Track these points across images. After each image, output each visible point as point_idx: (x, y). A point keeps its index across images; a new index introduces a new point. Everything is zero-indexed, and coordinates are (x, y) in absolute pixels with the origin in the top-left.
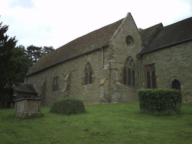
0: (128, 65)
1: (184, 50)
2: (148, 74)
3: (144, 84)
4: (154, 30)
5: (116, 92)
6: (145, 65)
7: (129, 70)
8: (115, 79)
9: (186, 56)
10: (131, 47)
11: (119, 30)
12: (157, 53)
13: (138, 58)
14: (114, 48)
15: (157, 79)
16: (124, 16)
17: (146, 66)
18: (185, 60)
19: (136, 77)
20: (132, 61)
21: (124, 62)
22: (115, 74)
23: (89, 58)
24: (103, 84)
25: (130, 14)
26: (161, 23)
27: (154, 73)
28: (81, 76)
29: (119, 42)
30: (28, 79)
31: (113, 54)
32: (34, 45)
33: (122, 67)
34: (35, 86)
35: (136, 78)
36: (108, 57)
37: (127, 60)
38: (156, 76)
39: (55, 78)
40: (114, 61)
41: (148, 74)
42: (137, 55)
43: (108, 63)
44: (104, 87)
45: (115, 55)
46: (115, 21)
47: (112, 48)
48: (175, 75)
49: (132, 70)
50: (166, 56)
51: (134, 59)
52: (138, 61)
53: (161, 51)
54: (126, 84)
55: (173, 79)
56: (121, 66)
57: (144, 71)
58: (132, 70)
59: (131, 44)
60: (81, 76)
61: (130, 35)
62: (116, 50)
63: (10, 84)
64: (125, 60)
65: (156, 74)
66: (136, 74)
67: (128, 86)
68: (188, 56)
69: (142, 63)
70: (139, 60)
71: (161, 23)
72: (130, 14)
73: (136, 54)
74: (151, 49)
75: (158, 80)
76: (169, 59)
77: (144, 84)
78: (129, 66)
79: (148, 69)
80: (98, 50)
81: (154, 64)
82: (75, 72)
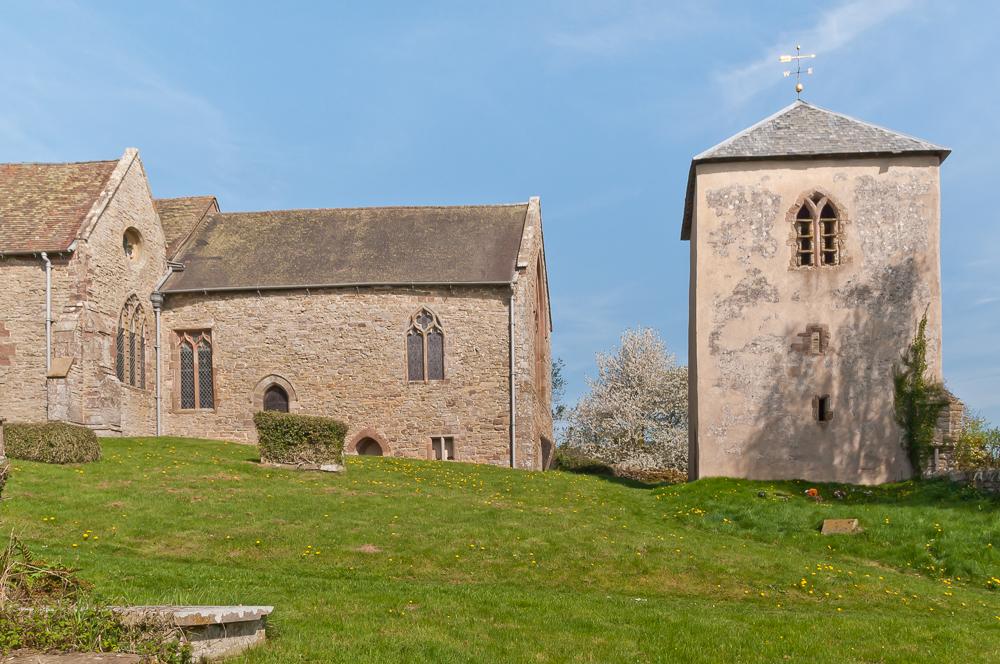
1: (304, 309)
5: (109, 402)
6: (176, 328)
7: (132, 336)
8: (101, 364)
9: (309, 326)
12: (222, 302)
13: (157, 305)
14: (92, 264)
15: (218, 376)
17: (180, 333)
18: (305, 336)
19: (147, 360)
22: (100, 347)
24: (64, 377)
27: (207, 357)
29: (104, 244)
31: (89, 282)
35: (149, 365)
36: (74, 291)
38: (214, 366)
40: (93, 305)
41: (186, 357)
43: (75, 311)
44: (67, 384)
45: (95, 287)
46: (697, 290)
47: (86, 264)
48: (275, 372)
50: (250, 315)
52: (155, 312)
55: (268, 382)
58: (137, 339)
61: (136, 226)
62: (97, 271)
67: (129, 388)
68: (314, 329)
70: (158, 310)
74: (203, 286)
75: (220, 379)
76: (259, 324)
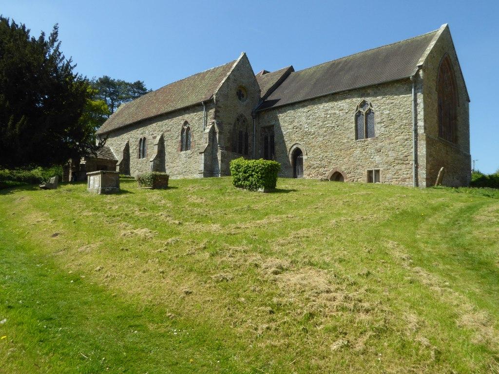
2: (266, 138)
7: (241, 132)
17: (264, 128)
23: (187, 117)
37: (238, 120)
49: (244, 133)
51: (247, 117)
54: (236, 152)
55: (295, 147)
66: (250, 138)
81: (273, 126)
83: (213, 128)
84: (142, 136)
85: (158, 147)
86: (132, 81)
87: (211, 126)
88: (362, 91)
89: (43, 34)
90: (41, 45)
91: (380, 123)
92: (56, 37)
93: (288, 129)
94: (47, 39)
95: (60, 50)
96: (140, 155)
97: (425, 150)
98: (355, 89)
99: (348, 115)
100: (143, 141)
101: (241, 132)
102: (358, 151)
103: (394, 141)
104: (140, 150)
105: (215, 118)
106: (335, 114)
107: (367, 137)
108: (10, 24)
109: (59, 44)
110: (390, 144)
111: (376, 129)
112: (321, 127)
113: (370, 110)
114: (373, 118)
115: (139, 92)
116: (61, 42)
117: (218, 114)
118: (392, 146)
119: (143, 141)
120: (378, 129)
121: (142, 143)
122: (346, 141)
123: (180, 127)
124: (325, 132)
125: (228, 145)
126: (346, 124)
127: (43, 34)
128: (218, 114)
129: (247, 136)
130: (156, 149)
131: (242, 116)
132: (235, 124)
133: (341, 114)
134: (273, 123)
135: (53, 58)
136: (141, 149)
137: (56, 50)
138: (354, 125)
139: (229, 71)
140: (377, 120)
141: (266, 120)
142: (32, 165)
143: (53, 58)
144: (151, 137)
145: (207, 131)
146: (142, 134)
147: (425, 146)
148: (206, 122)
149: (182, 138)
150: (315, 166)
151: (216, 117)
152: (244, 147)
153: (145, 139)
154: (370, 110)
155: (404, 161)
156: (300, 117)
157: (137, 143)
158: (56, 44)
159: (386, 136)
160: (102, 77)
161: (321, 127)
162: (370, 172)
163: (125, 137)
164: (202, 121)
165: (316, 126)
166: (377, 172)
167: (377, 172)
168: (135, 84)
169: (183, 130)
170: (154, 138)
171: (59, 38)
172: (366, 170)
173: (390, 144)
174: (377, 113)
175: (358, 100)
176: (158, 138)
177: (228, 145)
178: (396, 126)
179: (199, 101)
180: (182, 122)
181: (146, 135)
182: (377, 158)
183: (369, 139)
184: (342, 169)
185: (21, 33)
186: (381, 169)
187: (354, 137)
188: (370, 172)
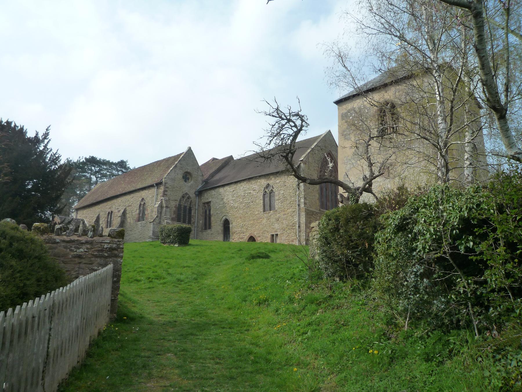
0: (183, 202)
2: (206, 211)
3: (201, 221)
4: (223, 162)
7: (185, 207)
10: (191, 183)
11: (176, 166)
12: (213, 191)
16: (185, 150)
17: (204, 203)
20: (189, 198)
21: (179, 200)
23: (144, 194)
25: (190, 150)
26: (232, 156)
28: (135, 212)
30: (79, 212)
32: (100, 156)
33: (176, 205)
34: (87, 221)
37: (183, 197)
39: (109, 213)
42: (195, 192)
49: (188, 207)
51: (191, 196)
53: (232, 185)
54: (180, 222)
55: (224, 218)
56: (175, 204)
57: (202, 209)
59: (190, 180)
60: (135, 212)
63: (448, 302)
64: (179, 198)
65: (212, 212)
66: (193, 212)
69: (201, 200)
71: (232, 156)
72: (190, 150)
73: (194, 191)
77: (201, 221)
78: (185, 203)
79: (205, 207)
80: (152, 186)
81: (210, 202)
82: (130, 207)
83: (162, 202)
84: (110, 211)
85: (121, 219)
86: (115, 160)
87: (160, 202)
88: (267, 176)
89: (37, 134)
90: (36, 141)
91: (278, 200)
92: (48, 136)
93: (220, 204)
94: (40, 136)
95: (48, 147)
96: (107, 225)
97: (304, 219)
98: (262, 175)
99: (258, 194)
100: (143, 207)
101: (185, 207)
102: (264, 221)
103: (286, 213)
104: (108, 221)
105: (163, 196)
106: (250, 193)
107: (270, 210)
108: (13, 125)
109: (48, 142)
110: (284, 215)
111: (276, 204)
112: (241, 203)
113: (272, 190)
114: (274, 196)
115: (122, 171)
116: (50, 140)
117: (166, 193)
118: (285, 216)
119: (110, 214)
120: (277, 205)
121: (109, 217)
122: (257, 213)
123: (139, 203)
124: (244, 206)
125: (174, 216)
126: (257, 201)
127: (37, 134)
128: (166, 193)
129: (190, 210)
130: (119, 220)
131: (186, 194)
132: (180, 200)
133: (254, 193)
134: (210, 200)
135: (42, 153)
136: (109, 220)
137: (45, 146)
138: (262, 201)
139: (176, 161)
140: (277, 198)
141: (208, 197)
142: (361, 211)
143: (42, 153)
144: (117, 211)
145: (157, 206)
146: (110, 208)
147: (304, 216)
148: (157, 199)
149: (140, 211)
150: (238, 232)
151: (164, 195)
152: (187, 218)
153: (112, 212)
154: (272, 190)
155: (293, 225)
156: (228, 195)
157: (106, 216)
158: (46, 141)
159: (282, 209)
160: (88, 157)
161: (241, 203)
162: (273, 235)
163: (97, 210)
164: (154, 198)
165: (238, 202)
166: (277, 235)
167: (277, 235)
168: (119, 163)
169: (141, 204)
170: (119, 211)
171: (49, 137)
172: (270, 234)
173: (284, 215)
174: (276, 193)
175: (263, 182)
176: (122, 211)
177: (174, 216)
178: (288, 202)
179: (152, 183)
180: (140, 199)
181: (113, 209)
182: (276, 226)
183: (272, 211)
184: (255, 234)
185: (22, 132)
186: (279, 233)
187: (262, 211)
188: (273, 235)
